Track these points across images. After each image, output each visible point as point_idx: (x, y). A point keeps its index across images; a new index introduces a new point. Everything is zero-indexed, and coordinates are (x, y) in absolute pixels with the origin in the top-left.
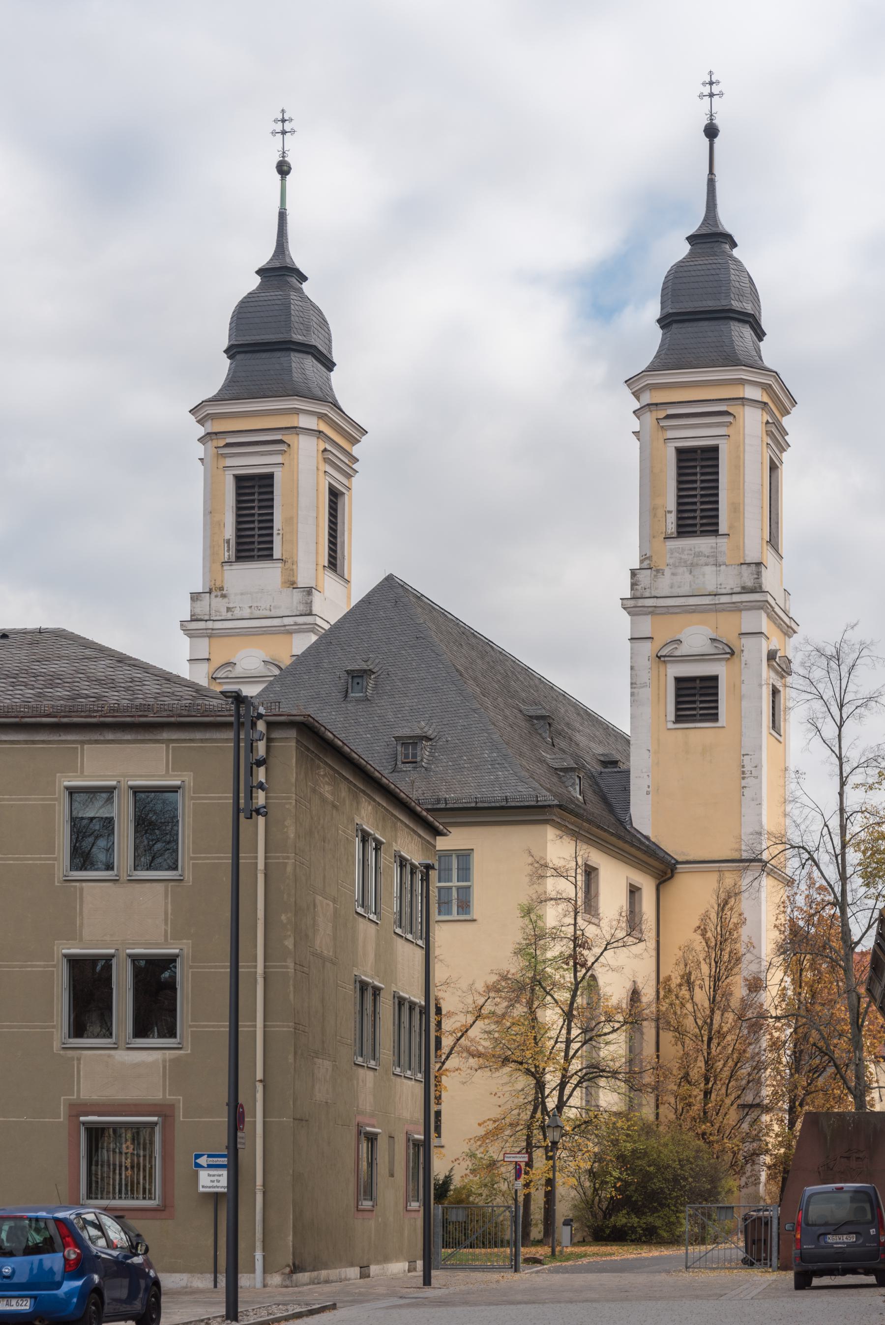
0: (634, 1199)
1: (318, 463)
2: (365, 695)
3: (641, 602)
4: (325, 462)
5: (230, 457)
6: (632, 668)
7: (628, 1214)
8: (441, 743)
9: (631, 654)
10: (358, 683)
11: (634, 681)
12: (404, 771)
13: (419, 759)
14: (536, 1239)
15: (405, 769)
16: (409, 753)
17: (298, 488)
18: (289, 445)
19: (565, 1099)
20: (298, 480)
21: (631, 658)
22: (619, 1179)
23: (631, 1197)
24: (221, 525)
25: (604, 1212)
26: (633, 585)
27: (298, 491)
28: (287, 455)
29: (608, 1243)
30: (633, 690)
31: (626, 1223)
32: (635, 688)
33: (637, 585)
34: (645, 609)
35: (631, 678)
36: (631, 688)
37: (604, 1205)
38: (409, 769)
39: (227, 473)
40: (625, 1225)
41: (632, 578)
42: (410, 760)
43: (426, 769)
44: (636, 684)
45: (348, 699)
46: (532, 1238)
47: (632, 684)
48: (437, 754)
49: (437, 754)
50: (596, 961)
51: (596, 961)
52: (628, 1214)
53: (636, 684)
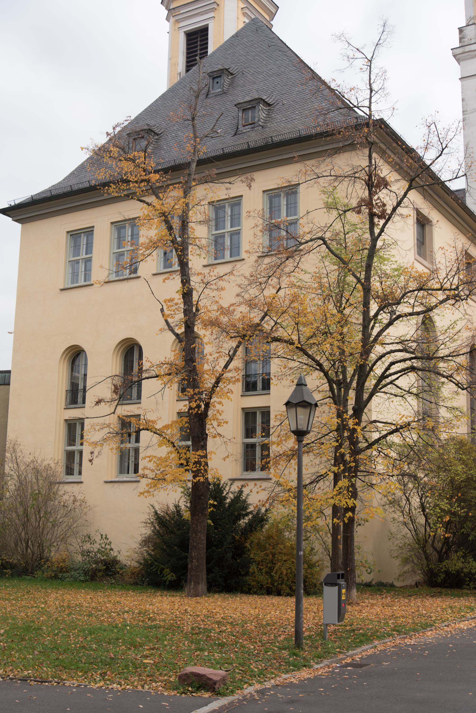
0: (470, 538)
1: (238, 15)
2: (222, 90)
3: (467, 48)
4: (244, 16)
5: (182, 21)
6: (463, 100)
7: (464, 557)
8: (278, 107)
9: (462, 89)
10: (217, 83)
11: (465, 109)
12: (244, 133)
13: (256, 119)
14: (364, 582)
15: (245, 131)
16: (249, 117)
17: (223, 31)
18: (218, 5)
19: (348, 380)
20: (224, 25)
21: (462, 93)
22: (449, 512)
23: (468, 535)
24: (176, 64)
25: (439, 553)
26: (461, 39)
27: (223, 33)
28: (217, 12)
29: (444, 590)
30: (465, 116)
31: (462, 569)
32: (466, 114)
33: (464, 38)
34: (472, 53)
35: (463, 108)
36: (463, 115)
37: (439, 545)
38: (248, 130)
39: (180, 31)
40: (459, 572)
41: (460, 34)
42: (250, 122)
43: (263, 127)
44: (466, 111)
45: (209, 96)
46: (358, 580)
47: (463, 112)
48: (273, 115)
49: (273, 115)
50: (399, 204)
51: (399, 204)
52: (464, 557)
53: (466, 111)
